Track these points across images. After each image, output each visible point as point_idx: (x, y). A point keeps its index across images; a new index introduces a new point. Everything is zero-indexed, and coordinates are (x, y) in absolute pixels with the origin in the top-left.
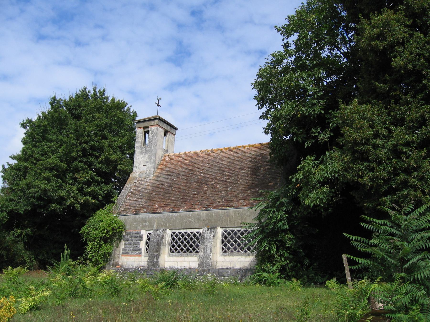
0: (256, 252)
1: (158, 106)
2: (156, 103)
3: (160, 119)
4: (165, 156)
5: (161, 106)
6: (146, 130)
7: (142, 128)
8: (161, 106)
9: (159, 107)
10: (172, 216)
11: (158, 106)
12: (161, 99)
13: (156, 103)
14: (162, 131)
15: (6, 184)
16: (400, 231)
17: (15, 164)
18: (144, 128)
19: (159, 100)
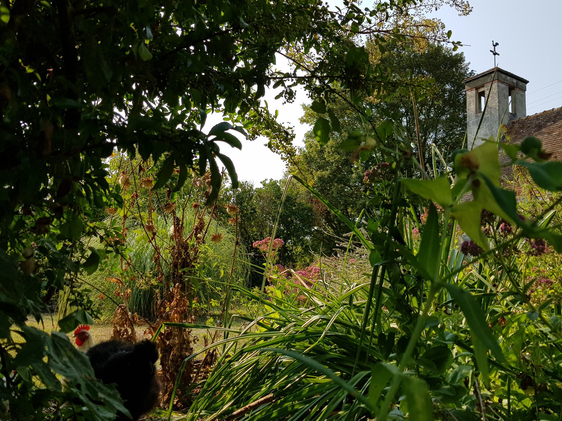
0: (314, 100)
1: (495, 54)
2: (491, 51)
3: (499, 71)
4: (514, 123)
5: (499, 55)
6: (481, 90)
7: (474, 89)
8: (499, 55)
9: (496, 55)
10: (161, 353)
11: (495, 54)
12: (497, 44)
13: (491, 51)
14: (504, 88)
15: (534, 249)
16: (155, 267)
17: (263, 183)
18: (477, 89)
19: (495, 46)
